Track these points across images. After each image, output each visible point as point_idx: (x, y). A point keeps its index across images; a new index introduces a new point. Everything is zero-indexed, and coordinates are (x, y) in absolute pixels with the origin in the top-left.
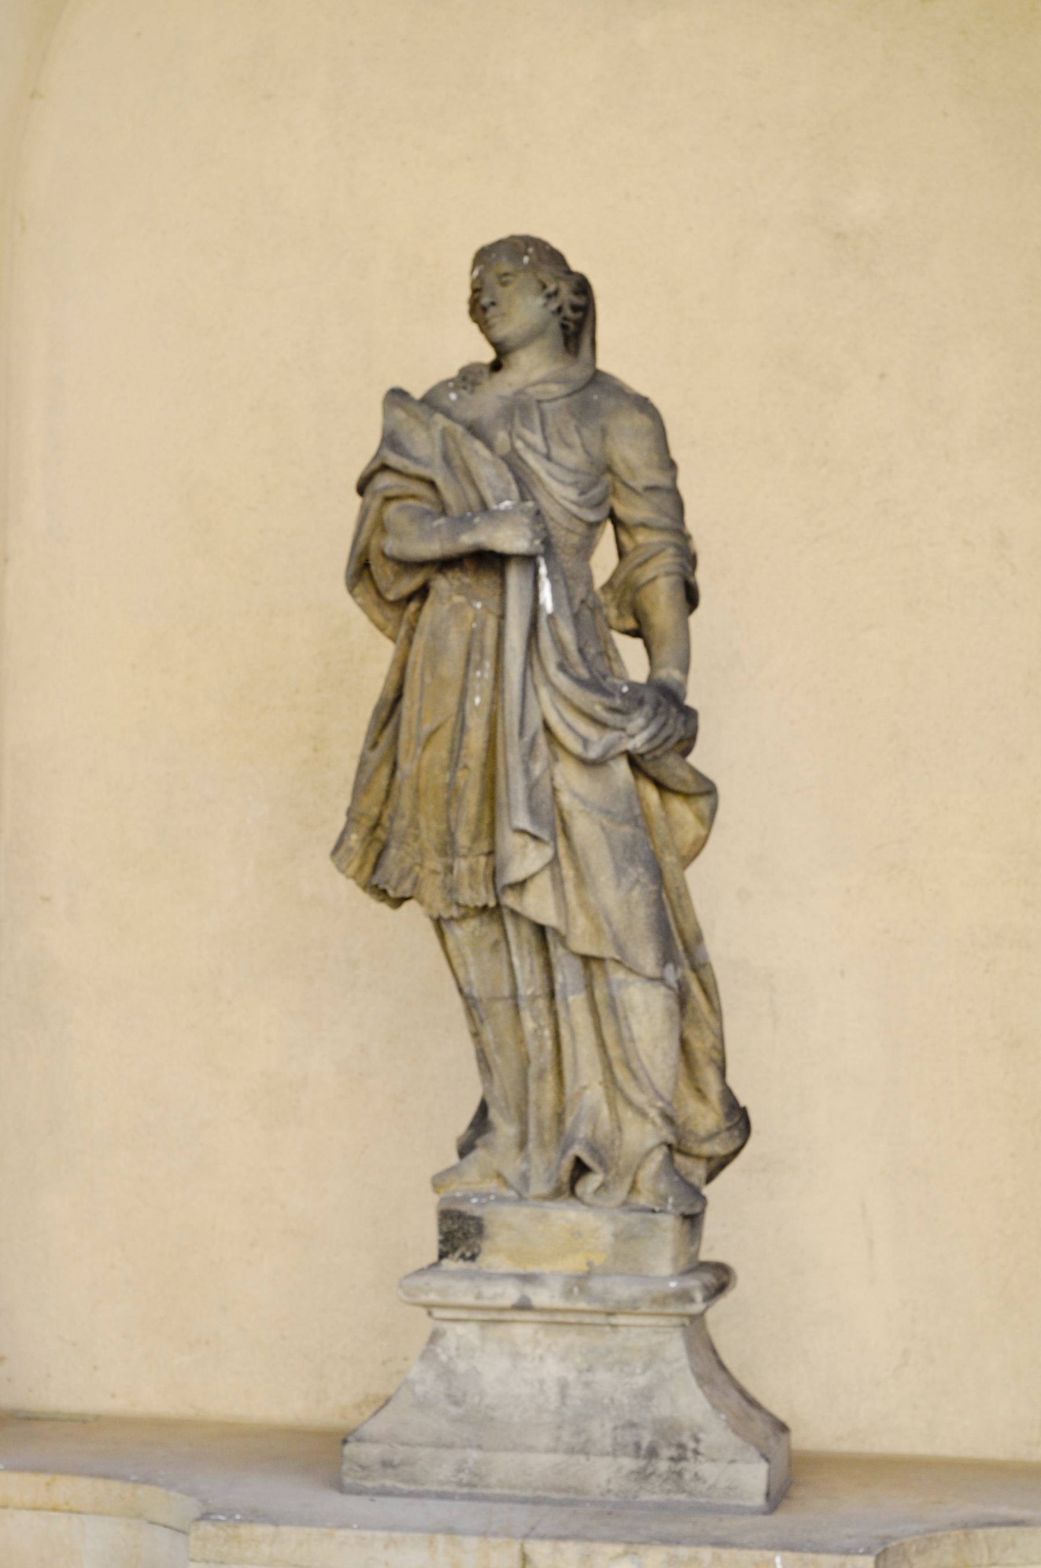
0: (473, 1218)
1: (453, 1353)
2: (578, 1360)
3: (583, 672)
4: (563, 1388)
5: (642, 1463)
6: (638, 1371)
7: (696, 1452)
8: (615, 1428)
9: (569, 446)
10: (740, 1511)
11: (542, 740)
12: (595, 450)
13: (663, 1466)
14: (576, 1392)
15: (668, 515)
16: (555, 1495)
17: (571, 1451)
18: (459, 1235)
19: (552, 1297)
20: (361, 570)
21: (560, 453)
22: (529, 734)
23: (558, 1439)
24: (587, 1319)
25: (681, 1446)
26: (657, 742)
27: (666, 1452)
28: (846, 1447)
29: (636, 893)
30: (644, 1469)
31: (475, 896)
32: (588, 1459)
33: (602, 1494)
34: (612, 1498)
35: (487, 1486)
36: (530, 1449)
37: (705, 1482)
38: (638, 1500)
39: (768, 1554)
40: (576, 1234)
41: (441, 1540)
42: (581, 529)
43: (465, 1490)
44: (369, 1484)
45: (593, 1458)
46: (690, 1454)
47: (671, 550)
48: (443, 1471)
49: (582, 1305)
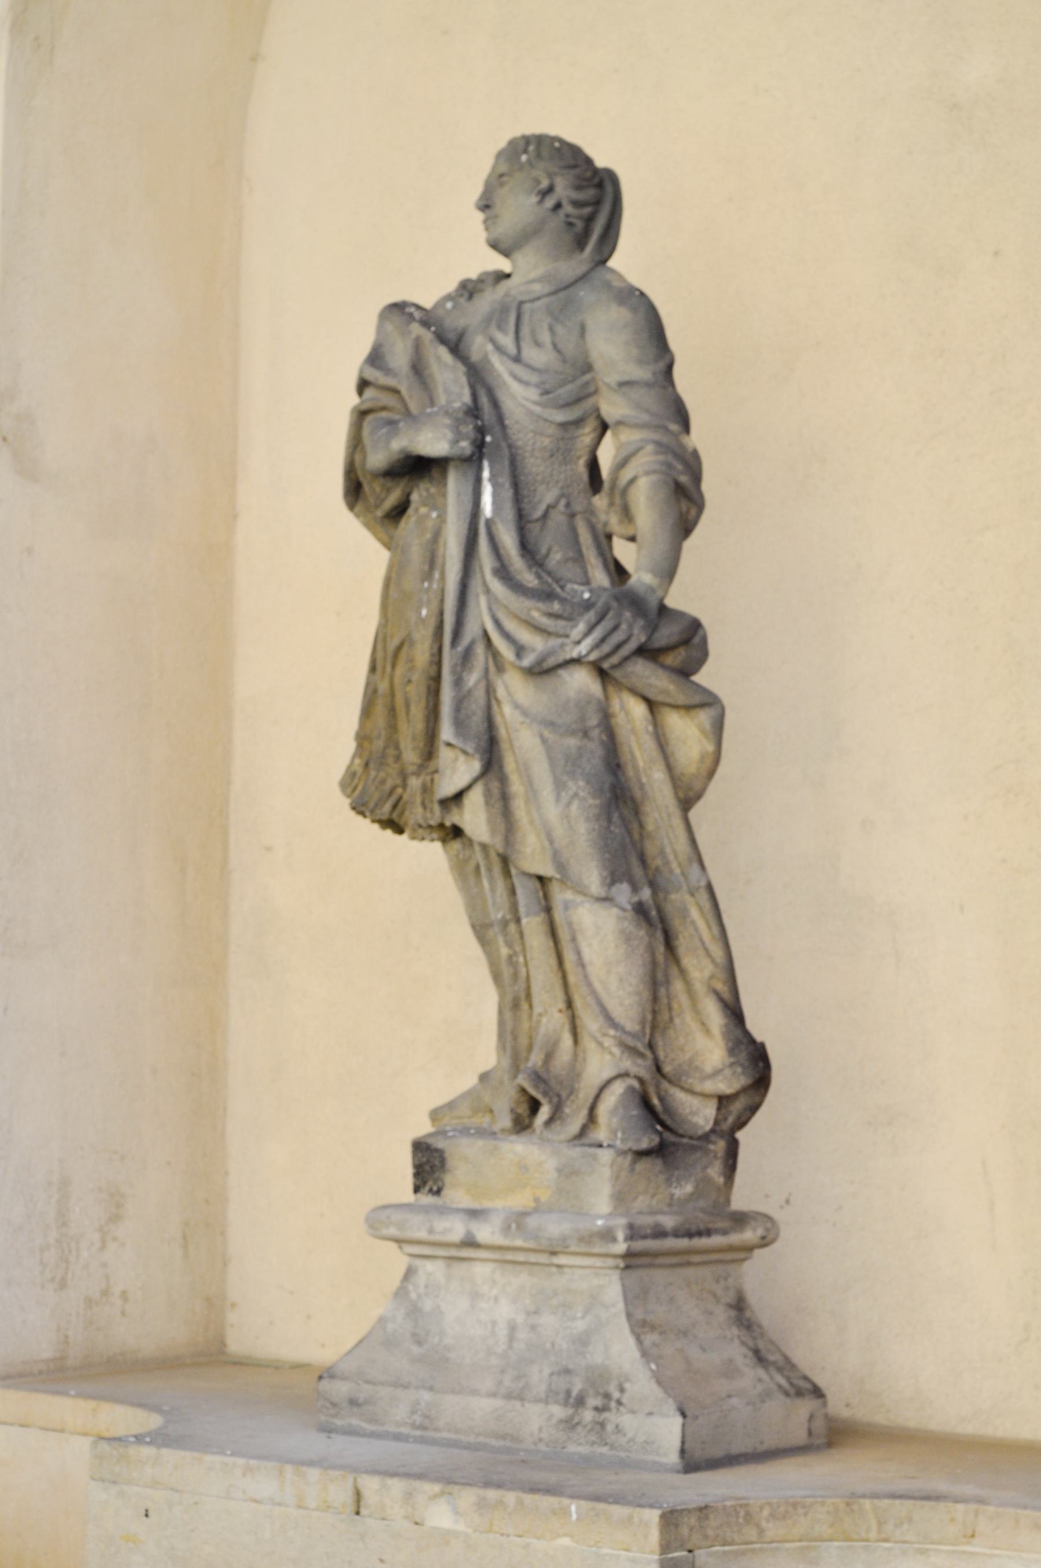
0: (437, 1150)
1: (422, 1290)
2: (527, 1301)
3: (529, 579)
4: (513, 1328)
5: (570, 1411)
6: (579, 1315)
7: (619, 1403)
8: (552, 1374)
9: (538, 344)
10: (658, 1468)
11: (480, 650)
12: (569, 347)
13: (588, 1415)
14: (522, 1335)
15: (647, 411)
16: (493, 1442)
17: (509, 1396)
18: (427, 1168)
19: (493, 1233)
20: (354, 490)
21: (530, 353)
22: (465, 642)
23: (500, 1383)
24: (520, 1257)
25: (607, 1396)
26: (606, 648)
27: (593, 1401)
28: (970, 1429)
29: (574, 807)
30: (572, 1418)
31: (429, 815)
32: (523, 1406)
33: (535, 1444)
34: (543, 1447)
35: (436, 1430)
36: (475, 1392)
37: (625, 1435)
38: (565, 1450)
39: (566, 1501)
40: (523, 1168)
41: (289, 1469)
42: (551, 430)
43: (418, 1433)
44: (339, 1422)
45: (527, 1405)
46: (613, 1404)
47: (650, 448)
48: (399, 1412)
49: (519, 1243)
